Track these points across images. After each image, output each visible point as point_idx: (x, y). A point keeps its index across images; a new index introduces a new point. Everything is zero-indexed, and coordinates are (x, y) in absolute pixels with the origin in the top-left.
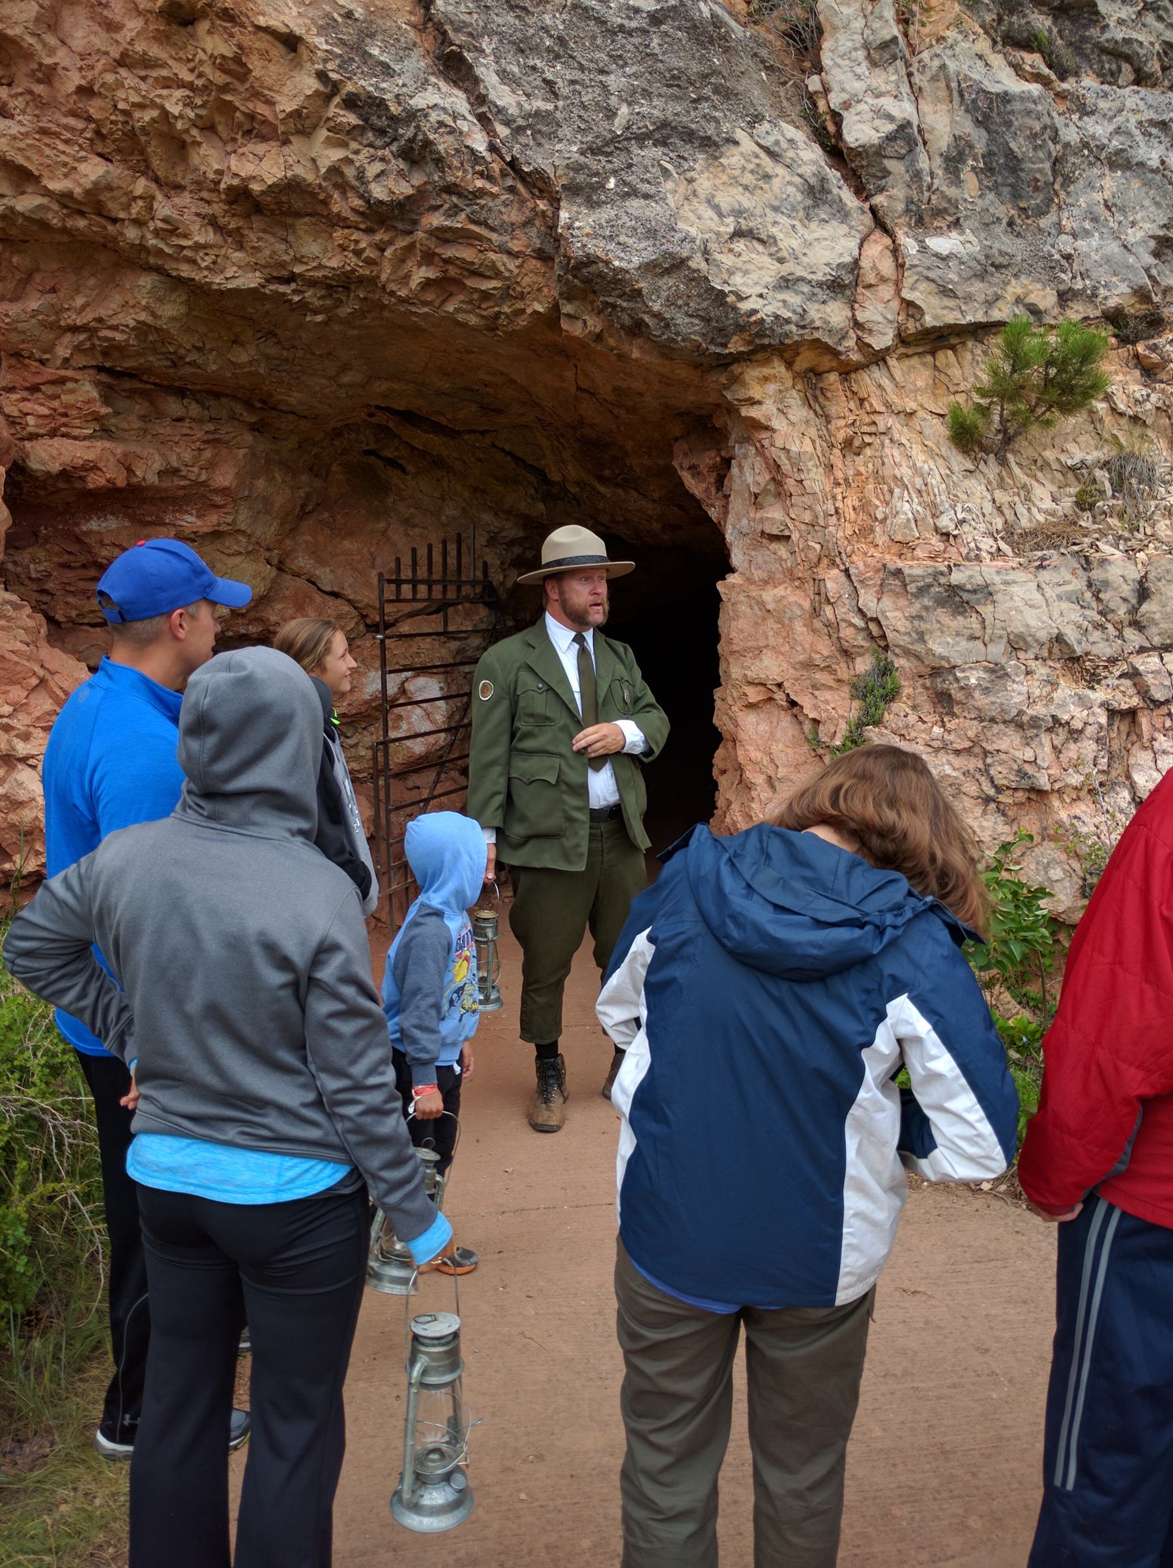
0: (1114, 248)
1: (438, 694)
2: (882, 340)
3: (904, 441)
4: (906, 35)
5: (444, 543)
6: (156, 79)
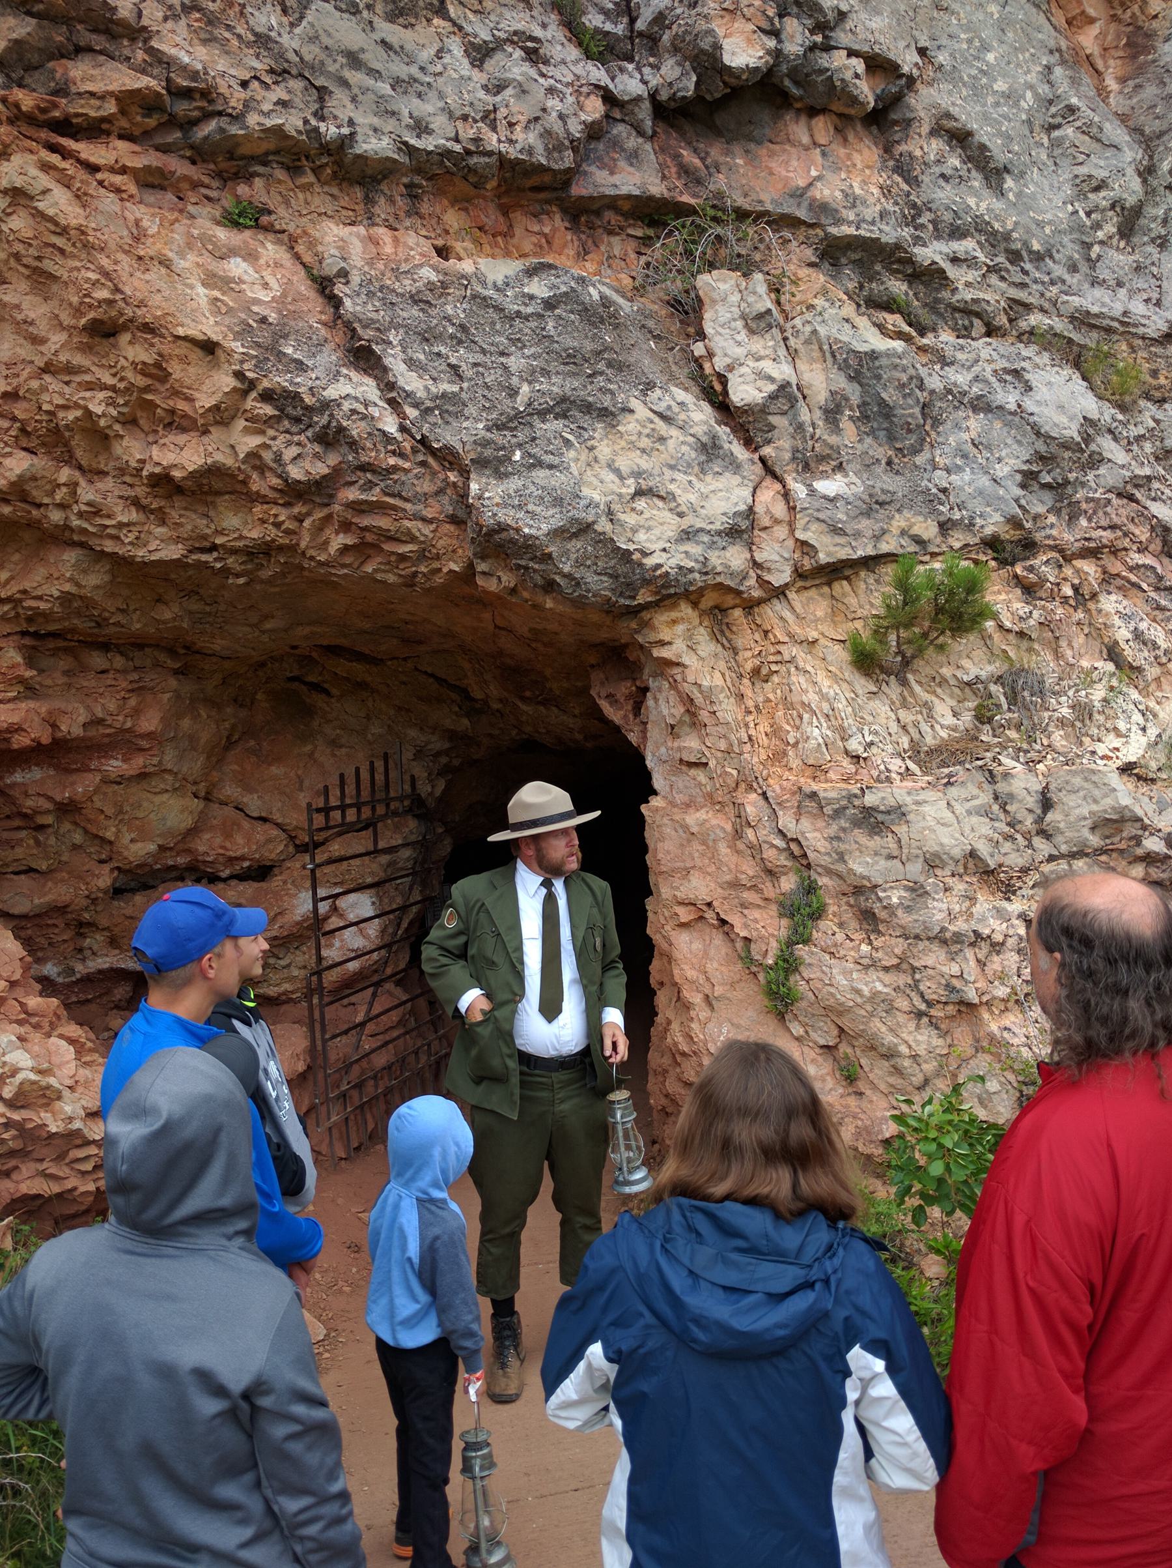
0: (984, 481)
2: (781, 576)
3: (809, 668)
4: (778, 303)
6: (79, 383)
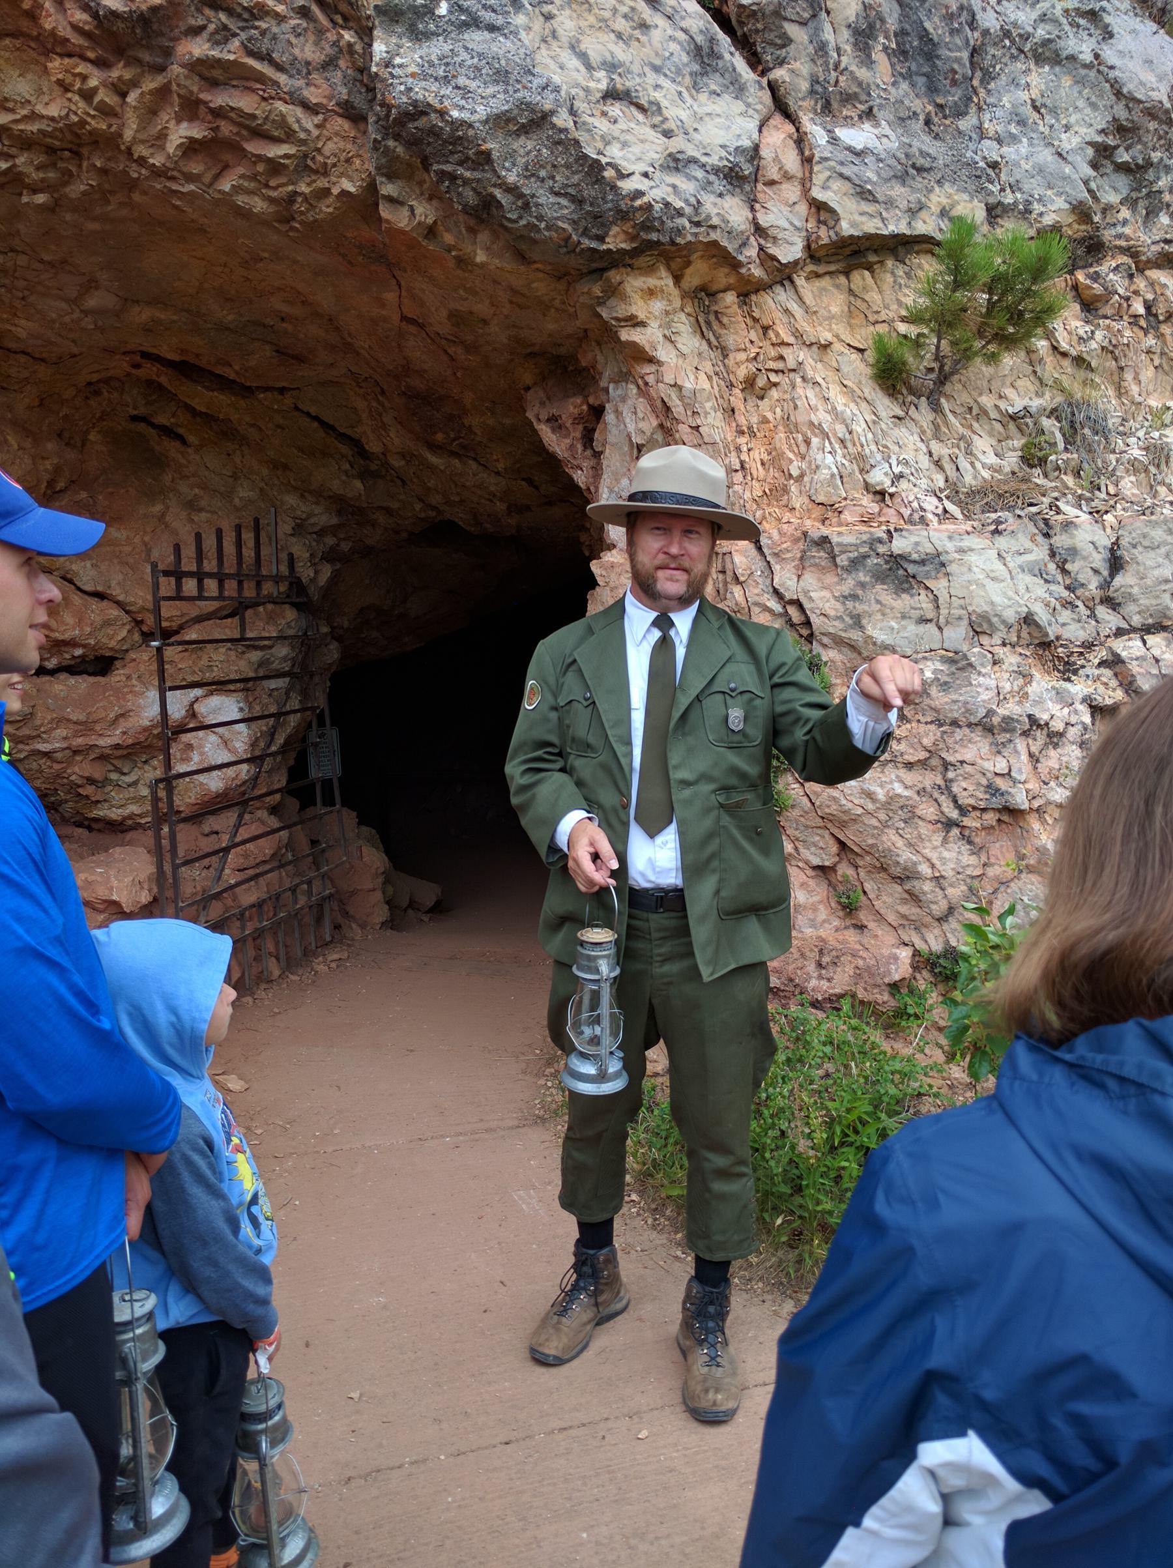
0: (1046, 156)
1: (236, 716)
2: (790, 251)
5: (238, 529)
